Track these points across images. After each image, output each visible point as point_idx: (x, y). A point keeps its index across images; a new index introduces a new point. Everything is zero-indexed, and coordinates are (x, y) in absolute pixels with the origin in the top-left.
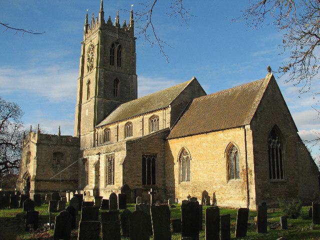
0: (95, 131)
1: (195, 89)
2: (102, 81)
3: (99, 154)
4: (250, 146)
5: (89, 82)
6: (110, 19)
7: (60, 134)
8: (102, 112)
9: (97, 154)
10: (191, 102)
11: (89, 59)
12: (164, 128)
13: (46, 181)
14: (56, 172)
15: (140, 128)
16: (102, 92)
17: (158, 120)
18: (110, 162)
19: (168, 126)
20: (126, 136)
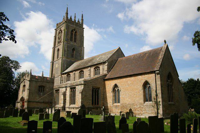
0: (61, 76)
1: (119, 53)
2: (66, 49)
3: (66, 87)
4: (159, 83)
5: (58, 50)
6: (71, 17)
7: (43, 75)
8: (66, 66)
11: (59, 38)
13: (34, 102)
15: (89, 74)
16: (66, 55)
17: (99, 69)
19: (105, 72)
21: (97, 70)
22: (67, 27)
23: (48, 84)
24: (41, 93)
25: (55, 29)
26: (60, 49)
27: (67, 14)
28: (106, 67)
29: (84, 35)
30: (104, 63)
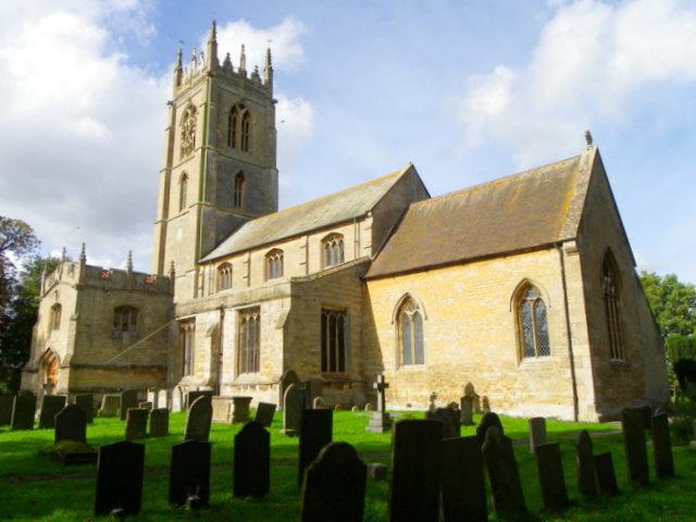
1: (411, 186)
2: (214, 174)
4: (576, 285)
5: (184, 177)
7: (130, 267)
8: (213, 235)
9: (217, 309)
10: (406, 209)
14: (120, 349)
15: (305, 259)
16: (214, 196)
18: (249, 317)
19: (366, 253)
25: (170, 103)
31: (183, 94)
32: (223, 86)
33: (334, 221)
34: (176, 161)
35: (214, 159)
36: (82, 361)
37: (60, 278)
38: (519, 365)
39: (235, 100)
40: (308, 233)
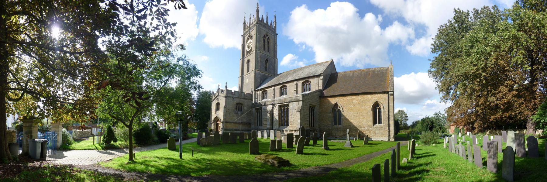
5: (248, 61)
6: (262, 17)
12: (317, 89)
16: (259, 67)
19: (321, 88)
20: (304, 90)
21: (265, 93)
22: (258, 32)
23: (246, 101)
24: (239, 112)
25: (242, 36)
26: (251, 60)
27: (258, 11)
28: (320, 81)
29: (277, 43)
30: (318, 76)
31: (247, 32)
32: (261, 28)
33: (307, 76)
34: (245, 56)
35: (259, 54)
36: (227, 120)
37: (219, 94)
38: (373, 126)
39: (265, 33)
40: (297, 80)
